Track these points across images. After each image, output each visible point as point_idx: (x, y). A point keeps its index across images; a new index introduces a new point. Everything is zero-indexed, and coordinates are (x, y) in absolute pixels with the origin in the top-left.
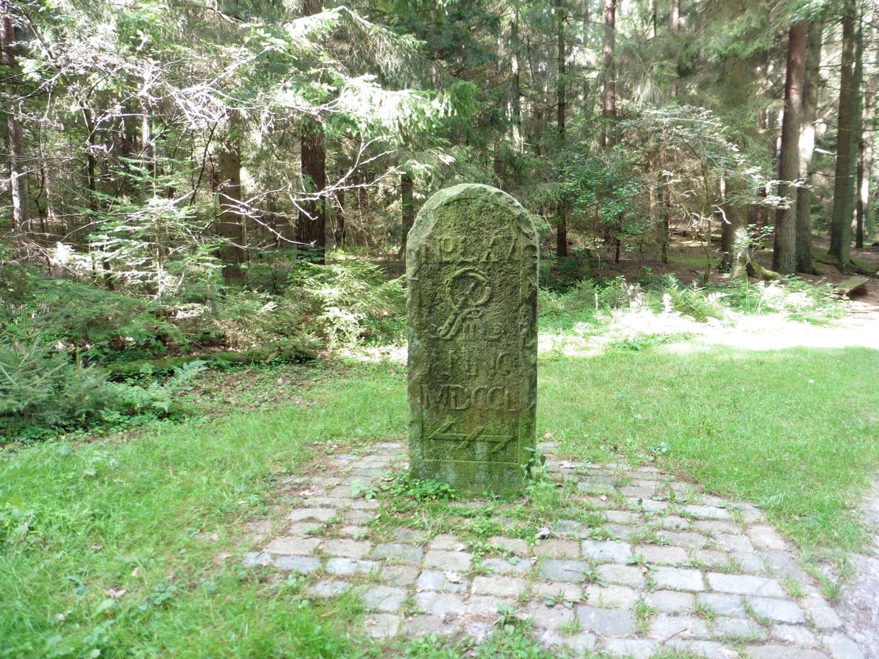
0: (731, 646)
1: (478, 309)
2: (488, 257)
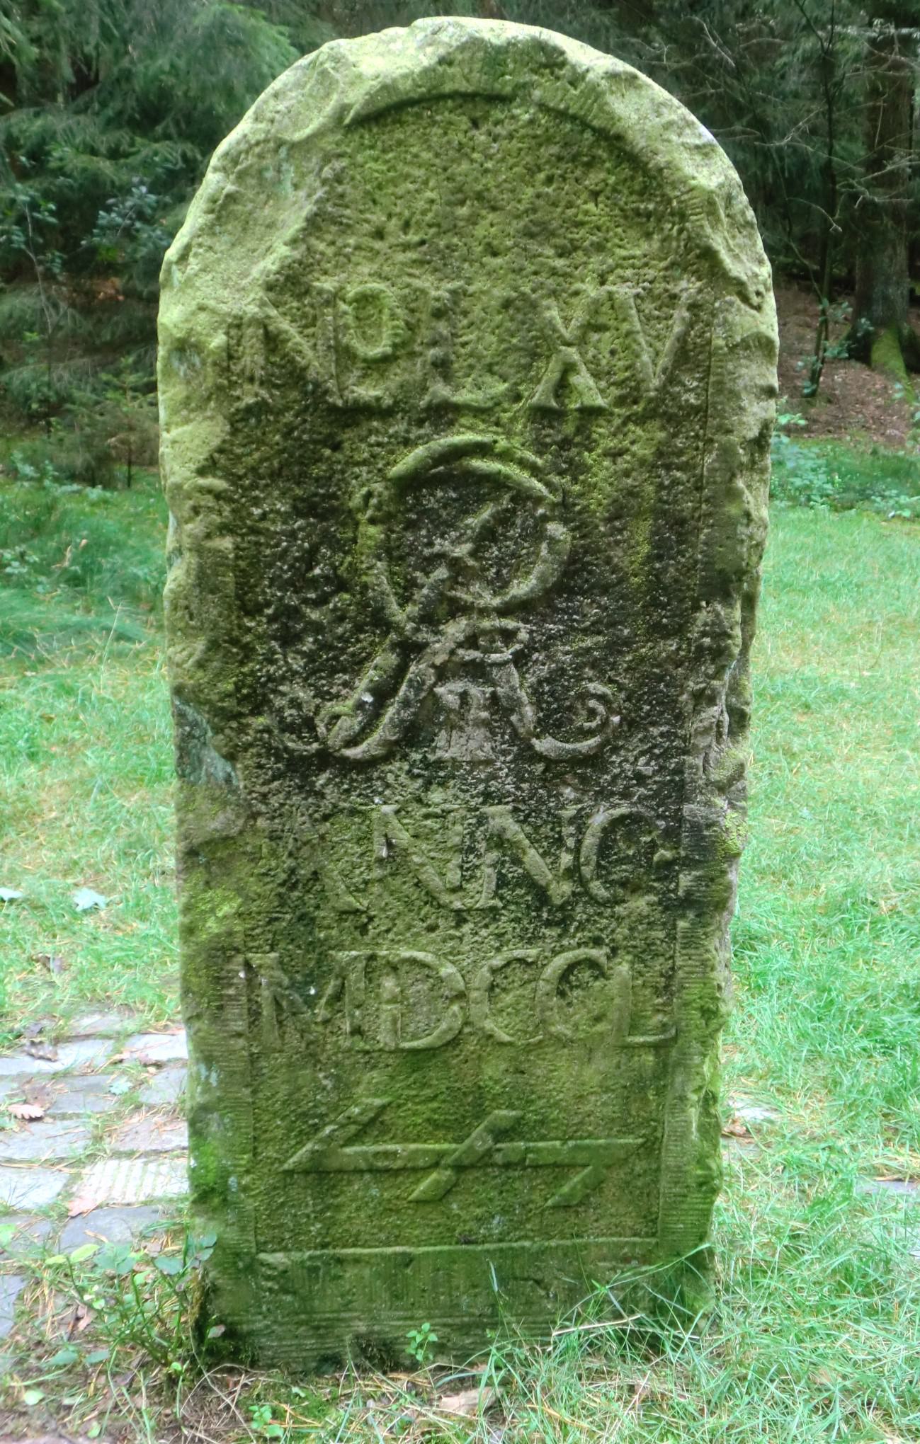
0: (677, 345)
1: (510, 623)
2: (249, 630)
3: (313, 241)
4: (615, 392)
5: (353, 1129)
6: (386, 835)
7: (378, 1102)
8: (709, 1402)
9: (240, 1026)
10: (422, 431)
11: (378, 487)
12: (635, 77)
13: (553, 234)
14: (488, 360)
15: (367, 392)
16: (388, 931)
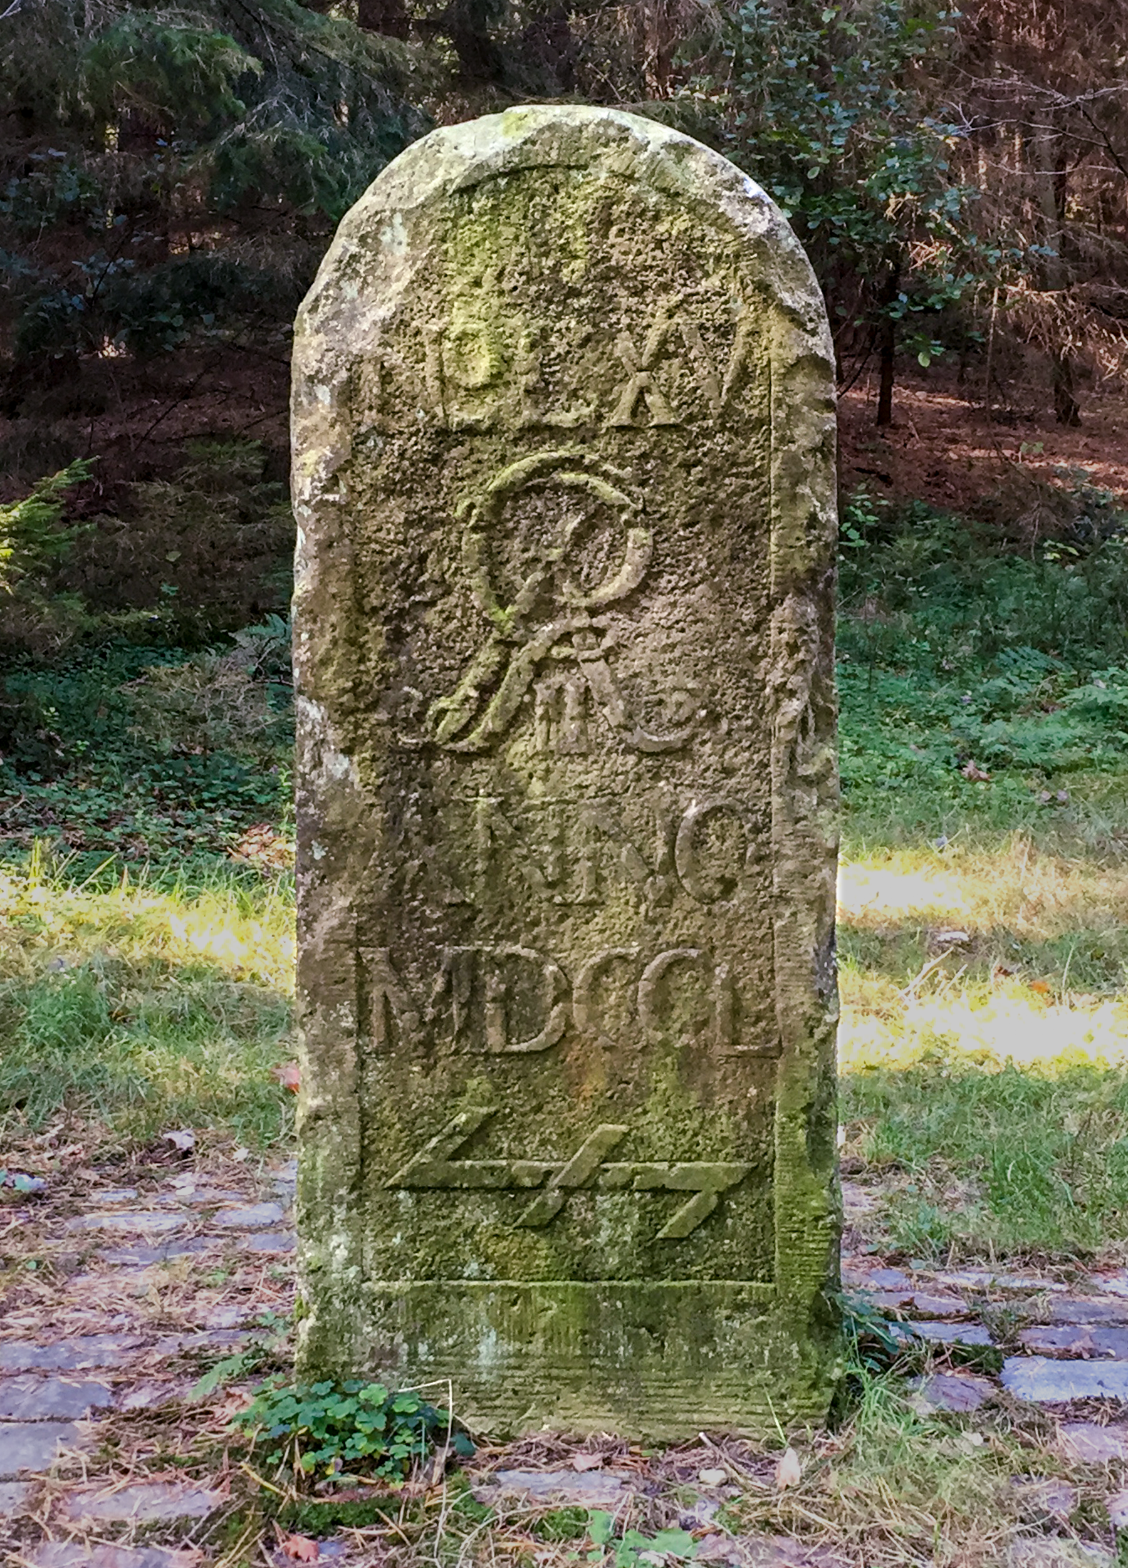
3: (421, 292)
4: (425, 67)
5: (459, 1140)
6: (490, 827)
7: (484, 1110)
8: (500, 277)
9: (349, 1023)
10: (517, 450)
11: (479, 499)
12: (691, 145)
13: (626, 277)
14: (573, 386)
15: (469, 416)
16: (491, 926)
